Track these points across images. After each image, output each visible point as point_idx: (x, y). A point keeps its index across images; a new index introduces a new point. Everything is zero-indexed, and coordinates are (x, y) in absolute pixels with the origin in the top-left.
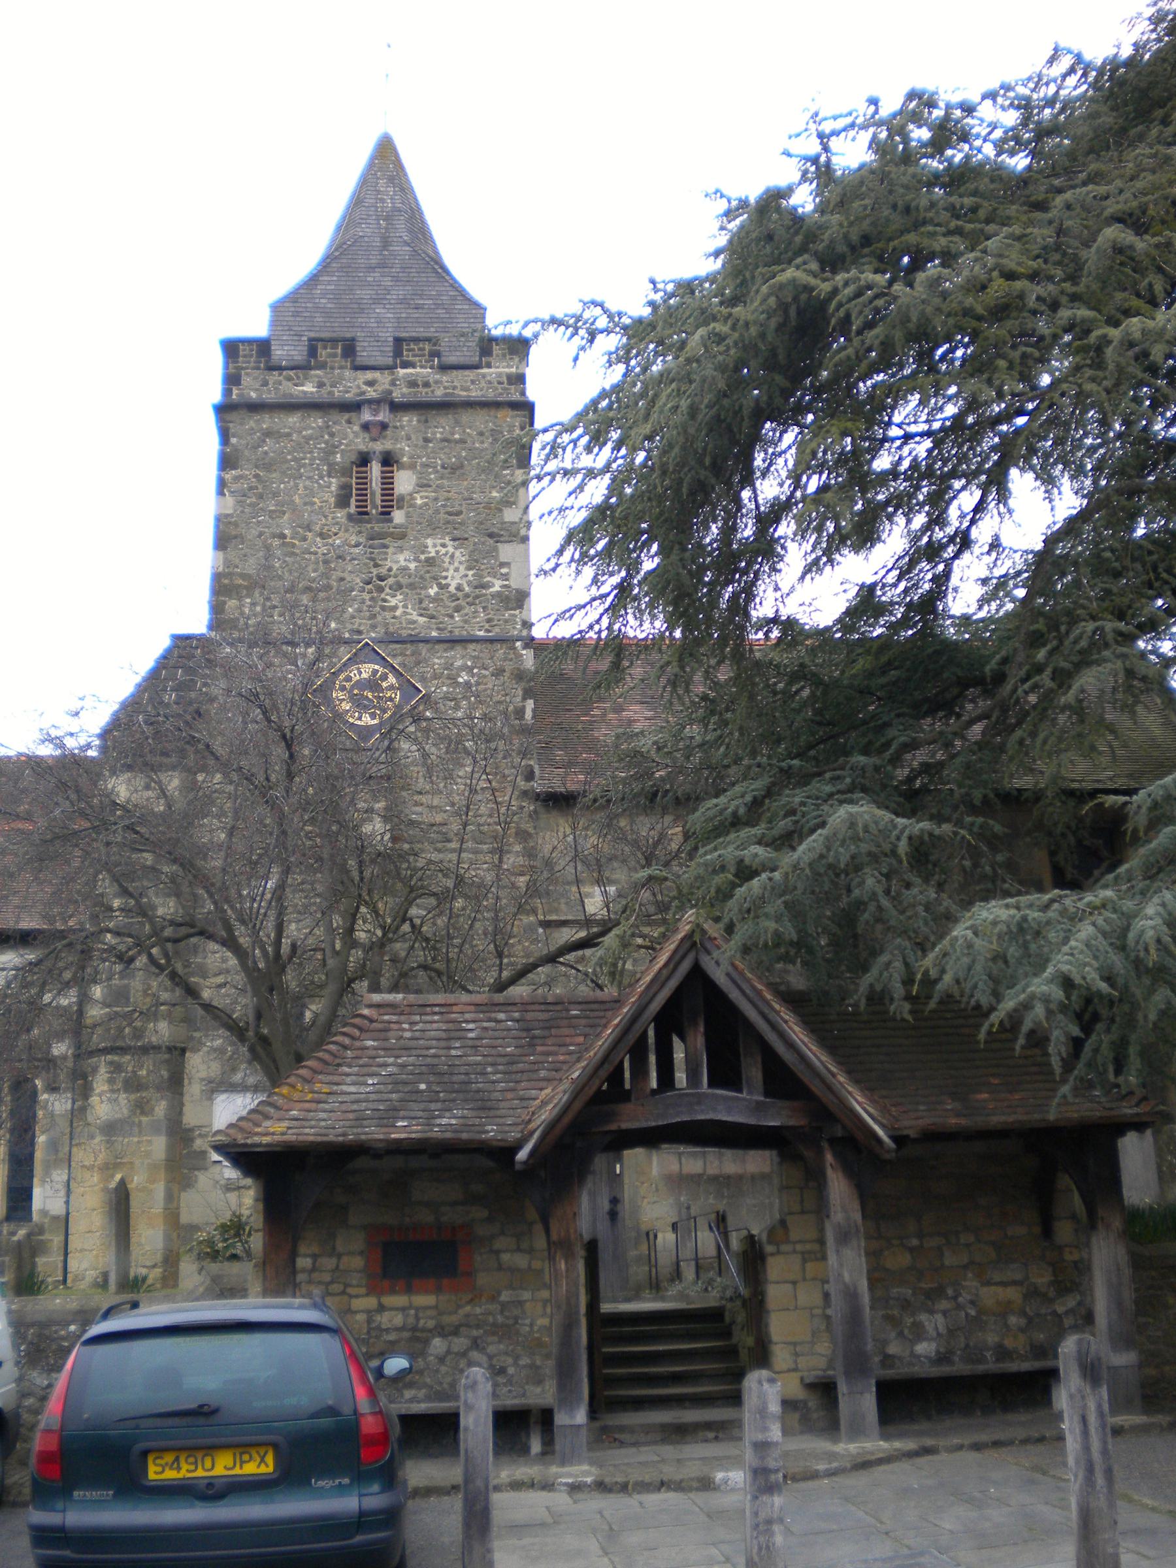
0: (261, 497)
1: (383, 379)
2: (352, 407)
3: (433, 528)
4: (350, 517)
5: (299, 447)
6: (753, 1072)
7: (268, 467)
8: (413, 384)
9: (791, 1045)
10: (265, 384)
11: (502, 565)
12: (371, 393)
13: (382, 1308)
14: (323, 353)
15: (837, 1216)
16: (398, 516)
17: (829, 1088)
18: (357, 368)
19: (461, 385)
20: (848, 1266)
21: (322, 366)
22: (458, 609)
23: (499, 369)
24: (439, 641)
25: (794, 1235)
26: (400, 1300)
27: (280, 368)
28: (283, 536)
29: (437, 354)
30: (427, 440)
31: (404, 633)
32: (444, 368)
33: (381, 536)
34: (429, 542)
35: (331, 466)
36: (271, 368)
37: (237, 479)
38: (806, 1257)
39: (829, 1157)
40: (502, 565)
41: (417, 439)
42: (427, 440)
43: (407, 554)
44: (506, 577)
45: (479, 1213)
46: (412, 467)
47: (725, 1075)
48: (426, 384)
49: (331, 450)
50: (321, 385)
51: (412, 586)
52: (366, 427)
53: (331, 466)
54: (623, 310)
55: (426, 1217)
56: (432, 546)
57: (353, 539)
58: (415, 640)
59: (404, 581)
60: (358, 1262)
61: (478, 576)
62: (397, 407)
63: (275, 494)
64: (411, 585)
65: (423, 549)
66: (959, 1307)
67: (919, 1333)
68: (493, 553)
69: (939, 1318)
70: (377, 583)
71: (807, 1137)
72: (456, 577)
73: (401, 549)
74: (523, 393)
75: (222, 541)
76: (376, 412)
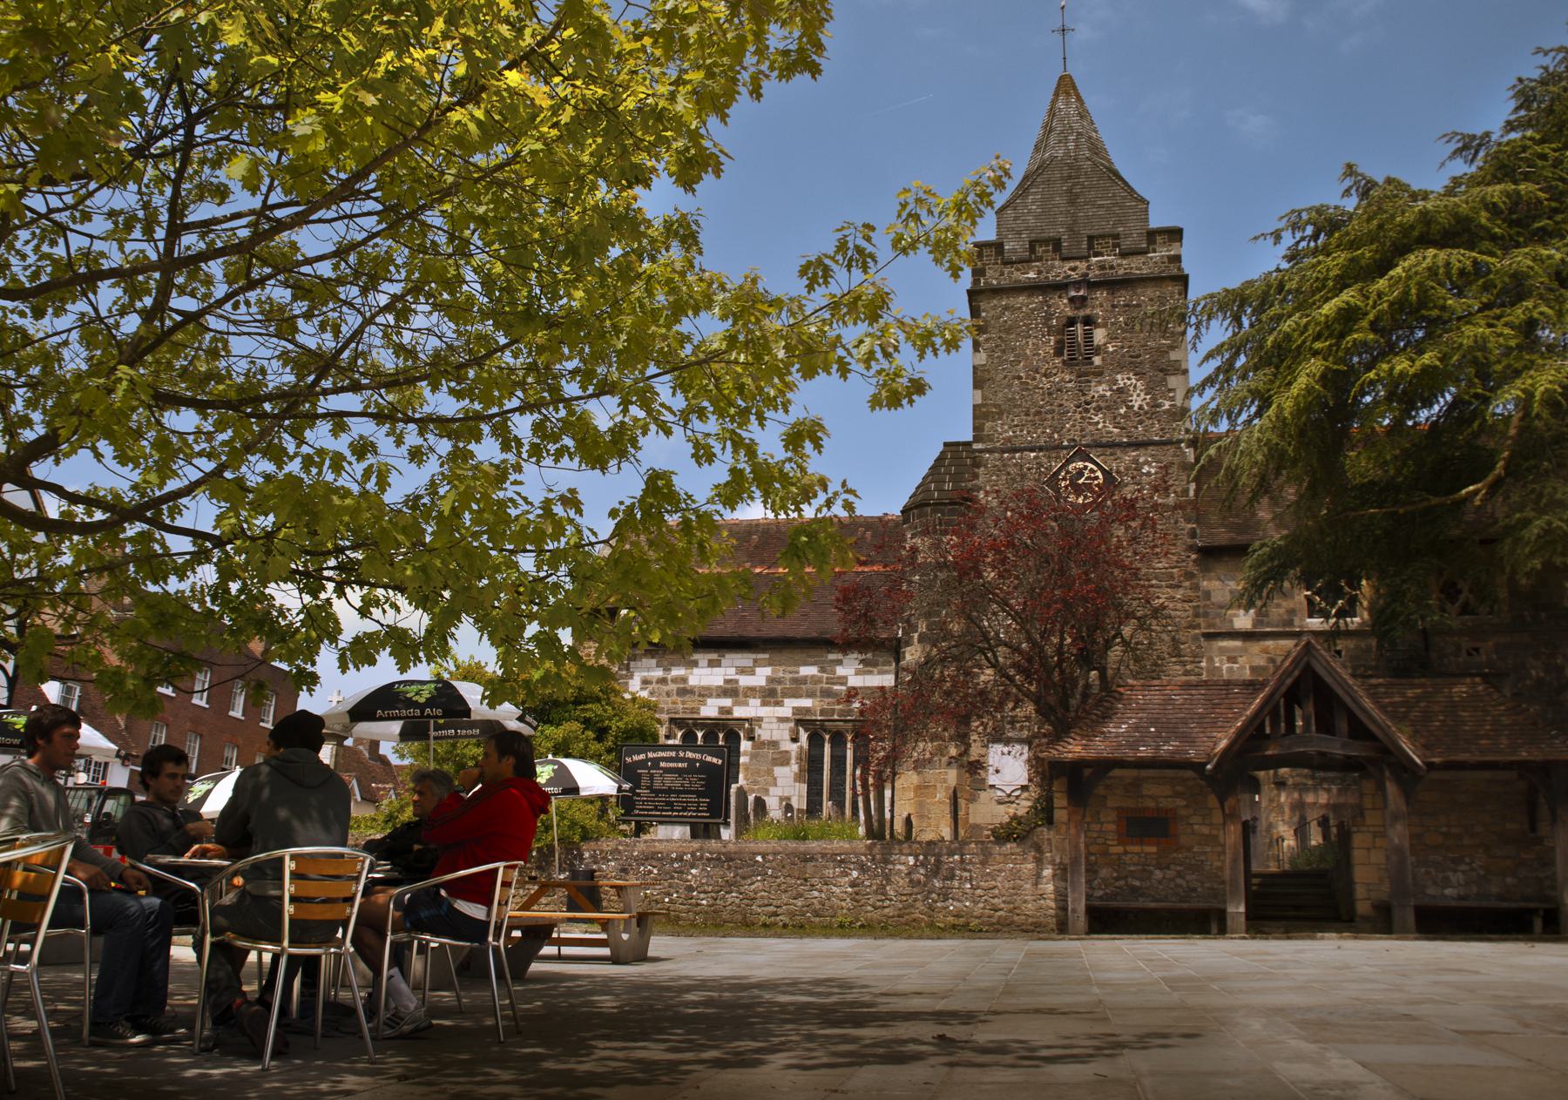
0: (1004, 351)
1: (1082, 265)
2: (1061, 287)
3: (1121, 367)
4: (1064, 362)
5: (1028, 316)
6: (1342, 725)
7: (1008, 331)
8: (1102, 268)
9: (1364, 710)
10: (1002, 274)
11: (1170, 390)
12: (1074, 276)
13: (1126, 853)
14: (1040, 250)
15: (1392, 806)
16: (1097, 360)
17: (1387, 735)
18: (1064, 259)
19: (1136, 266)
20: (1399, 834)
21: (1040, 259)
22: (1141, 422)
23: (1161, 252)
24: (1129, 445)
25: (1369, 822)
26: (1136, 849)
27: (1012, 263)
28: (1020, 378)
29: (1118, 245)
30: (1114, 306)
31: (1104, 440)
32: (1123, 255)
33: (1086, 374)
34: (1119, 377)
35: (1049, 327)
36: (1005, 263)
37: (987, 340)
38: (1375, 835)
39: (1387, 774)
40: (1170, 390)
41: (1107, 305)
42: (1114, 306)
43: (1104, 386)
44: (1172, 399)
45: (1181, 802)
46: (1105, 325)
47: (1325, 725)
48: (1112, 267)
49: (1048, 317)
50: (1039, 272)
51: (1108, 408)
52: (1072, 300)
53: (1049, 327)
54: (894, 414)
55: (1151, 804)
56: (1121, 379)
57: (1067, 378)
58: (1113, 445)
59: (1103, 404)
60: (1113, 827)
61: (1154, 399)
62: (1093, 286)
63: (1014, 349)
64: (1107, 407)
65: (1115, 382)
66: (1473, 870)
67: (1446, 882)
68: (1164, 381)
69: (1460, 876)
70: (1084, 407)
71: (1371, 761)
72: (1138, 400)
73: (1100, 383)
74: (1180, 269)
75: (978, 384)
76: (1078, 290)
